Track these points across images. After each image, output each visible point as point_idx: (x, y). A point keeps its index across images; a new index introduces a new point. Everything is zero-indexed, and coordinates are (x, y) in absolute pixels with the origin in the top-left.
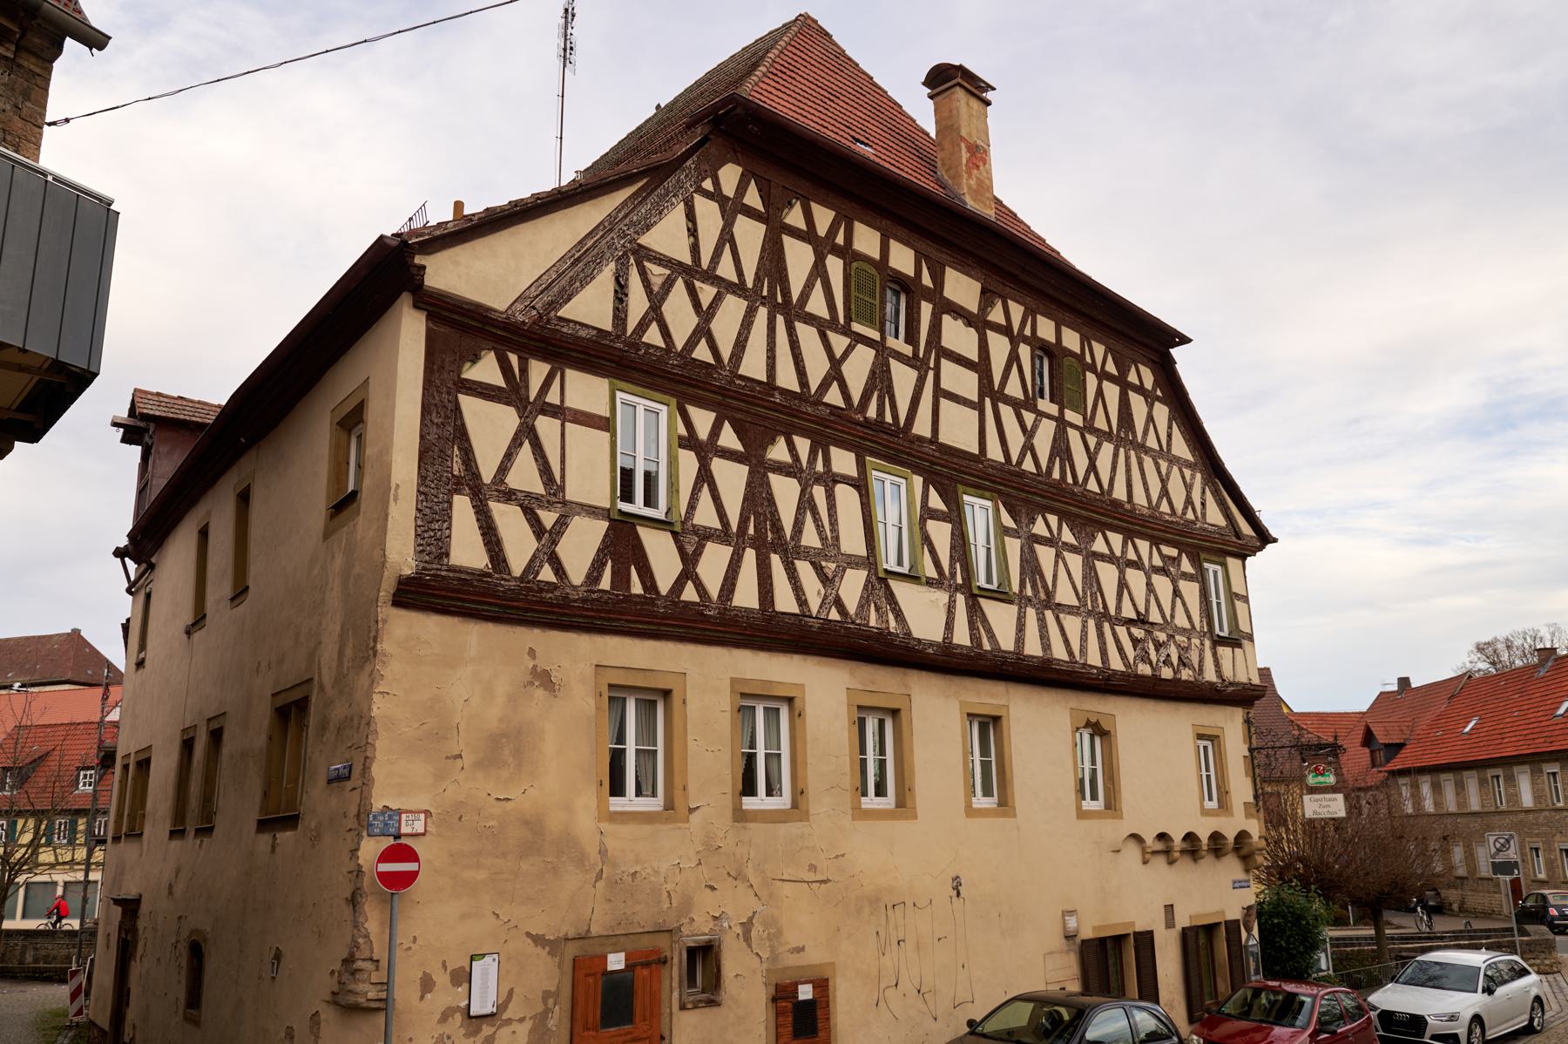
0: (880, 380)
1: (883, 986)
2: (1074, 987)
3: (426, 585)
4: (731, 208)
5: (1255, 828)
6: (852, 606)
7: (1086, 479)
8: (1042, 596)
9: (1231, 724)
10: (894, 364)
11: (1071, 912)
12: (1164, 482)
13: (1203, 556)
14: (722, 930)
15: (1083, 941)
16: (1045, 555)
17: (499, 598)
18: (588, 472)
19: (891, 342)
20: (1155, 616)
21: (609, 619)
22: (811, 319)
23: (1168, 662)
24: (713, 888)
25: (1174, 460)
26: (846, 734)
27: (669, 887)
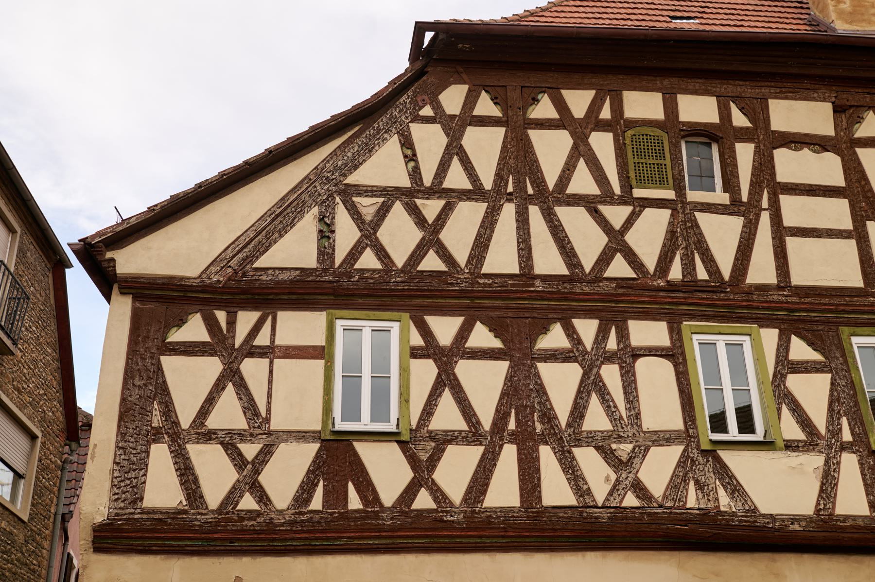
0: (684, 236)
3: (120, 530)
4: (455, 127)
10: (702, 218)
17: (196, 532)
18: (295, 396)
19: (693, 196)
21: (327, 539)
22: (576, 200)
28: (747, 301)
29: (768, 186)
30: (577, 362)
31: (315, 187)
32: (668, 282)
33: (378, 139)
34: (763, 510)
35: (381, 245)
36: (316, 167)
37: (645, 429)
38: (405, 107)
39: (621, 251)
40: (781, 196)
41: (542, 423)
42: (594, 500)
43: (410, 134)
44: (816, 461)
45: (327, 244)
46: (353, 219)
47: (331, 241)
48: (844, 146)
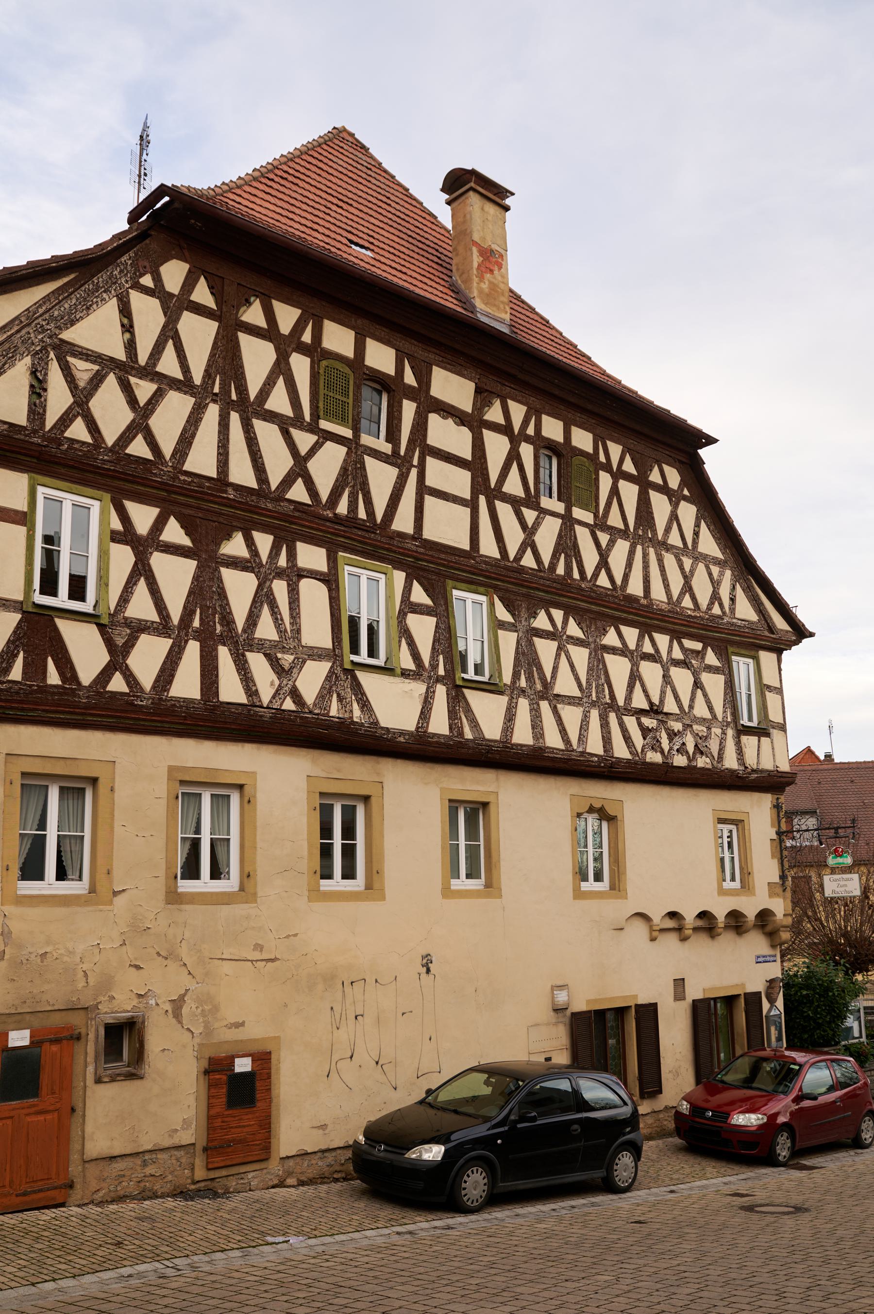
0: (352, 476)
1: (335, 1057)
2: (562, 1058)
4: (175, 306)
5: (780, 907)
6: (310, 695)
7: (596, 575)
8: (539, 687)
9: (758, 810)
10: (369, 461)
11: (561, 987)
12: (687, 579)
13: (730, 649)
14: (148, 1007)
15: (572, 1014)
16: (546, 649)
19: (366, 440)
20: (670, 706)
21: (23, 709)
22: (271, 417)
23: (682, 750)
24: (138, 967)
25: (699, 557)
26: (304, 820)
27: (85, 967)
28: (389, 544)
29: (420, 446)
30: (254, 572)
31: (29, 333)
32: (335, 514)
33: (97, 297)
34: (383, 724)
35: (92, 417)
36: (28, 309)
37: (304, 644)
38: (126, 268)
39: (302, 477)
40: (428, 457)
41: (222, 625)
42: (260, 701)
43: (129, 301)
44: (419, 688)
45: (38, 401)
46: (67, 381)
47: (43, 399)
48: (475, 424)
